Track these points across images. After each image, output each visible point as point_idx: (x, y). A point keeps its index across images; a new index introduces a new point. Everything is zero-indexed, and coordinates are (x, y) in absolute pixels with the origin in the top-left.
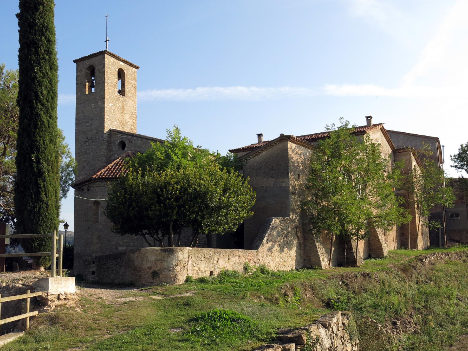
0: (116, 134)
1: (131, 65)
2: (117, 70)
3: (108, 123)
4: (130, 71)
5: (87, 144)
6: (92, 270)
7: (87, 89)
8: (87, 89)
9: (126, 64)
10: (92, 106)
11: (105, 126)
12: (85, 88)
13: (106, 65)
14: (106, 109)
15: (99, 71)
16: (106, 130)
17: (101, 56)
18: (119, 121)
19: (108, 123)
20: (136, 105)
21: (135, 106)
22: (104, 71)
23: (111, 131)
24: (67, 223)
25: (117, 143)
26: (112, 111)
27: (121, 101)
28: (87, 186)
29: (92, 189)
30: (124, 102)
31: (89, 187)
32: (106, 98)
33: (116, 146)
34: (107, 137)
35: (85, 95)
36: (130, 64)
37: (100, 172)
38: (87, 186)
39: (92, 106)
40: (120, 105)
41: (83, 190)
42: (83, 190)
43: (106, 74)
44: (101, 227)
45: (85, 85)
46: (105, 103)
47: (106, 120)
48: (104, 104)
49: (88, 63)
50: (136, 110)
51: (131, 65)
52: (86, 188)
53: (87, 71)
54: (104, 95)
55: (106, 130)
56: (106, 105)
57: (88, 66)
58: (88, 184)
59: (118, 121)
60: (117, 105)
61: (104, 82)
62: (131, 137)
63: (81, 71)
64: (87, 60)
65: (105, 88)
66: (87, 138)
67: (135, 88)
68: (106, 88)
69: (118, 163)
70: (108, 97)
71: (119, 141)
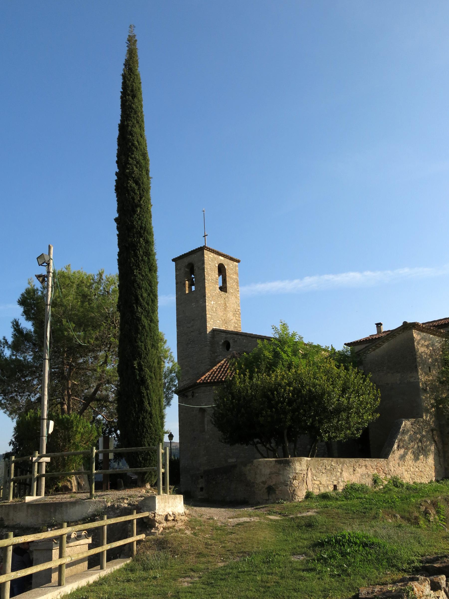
0: (219, 333)
1: (232, 259)
2: (217, 265)
3: (211, 322)
4: (231, 265)
5: (190, 346)
6: (200, 486)
7: (187, 288)
8: (187, 288)
9: (226, 258)
10: (193, 305)
11: (207, 325)
12: (185, 287)
13: (205, 261)
14: (207, 307)
15: (199, 268)
16: (209, 330)
17: (200, 252)
18: (222, 319)
19: (211, 322)
20: (239, 301)
21: (238, 303)
22: (204, 268)
23: (214, 331)
24: (172, 433)
25: (221, 343)
26: (214, 309)
27: (223, 298)
28: (191, 392)
29: (197, 394)
30: (226, 299)
31: (193, 392)
32: (207, 296)
33: (220, 347)
34: (210, 338)
35: (186, 294)
36: (231, 258)
37: (205, 376)
38: (191, 392)
39: (193, 305)
40: (223, 302)
41: (187, 396)
42: (187, 396)
43: (205, 270)
44: (208, 437)
45: (185, 284)
46: (207, 301)
47: (208, 320)
48: (205, 302)
49: (186, 261)
50: (239, 307)
51: (232, 259)
52: (190, 394)
53: (186, 269)
54: (205, 292)
55: (209, 330)
56: (207, 304)
57: (187, 264)
58: (192, 390)
59: (220, 320)
60: (219, 302)
61: (204, 279)
62: (235, 336)
63: (180, 269)
64: (185, 258)
65: (206, 286)
66: (189, 340)
67: (237, 283)
68: (207, 285)
69: (223, 365)
70: (209, 294)
71: (223, 341)
